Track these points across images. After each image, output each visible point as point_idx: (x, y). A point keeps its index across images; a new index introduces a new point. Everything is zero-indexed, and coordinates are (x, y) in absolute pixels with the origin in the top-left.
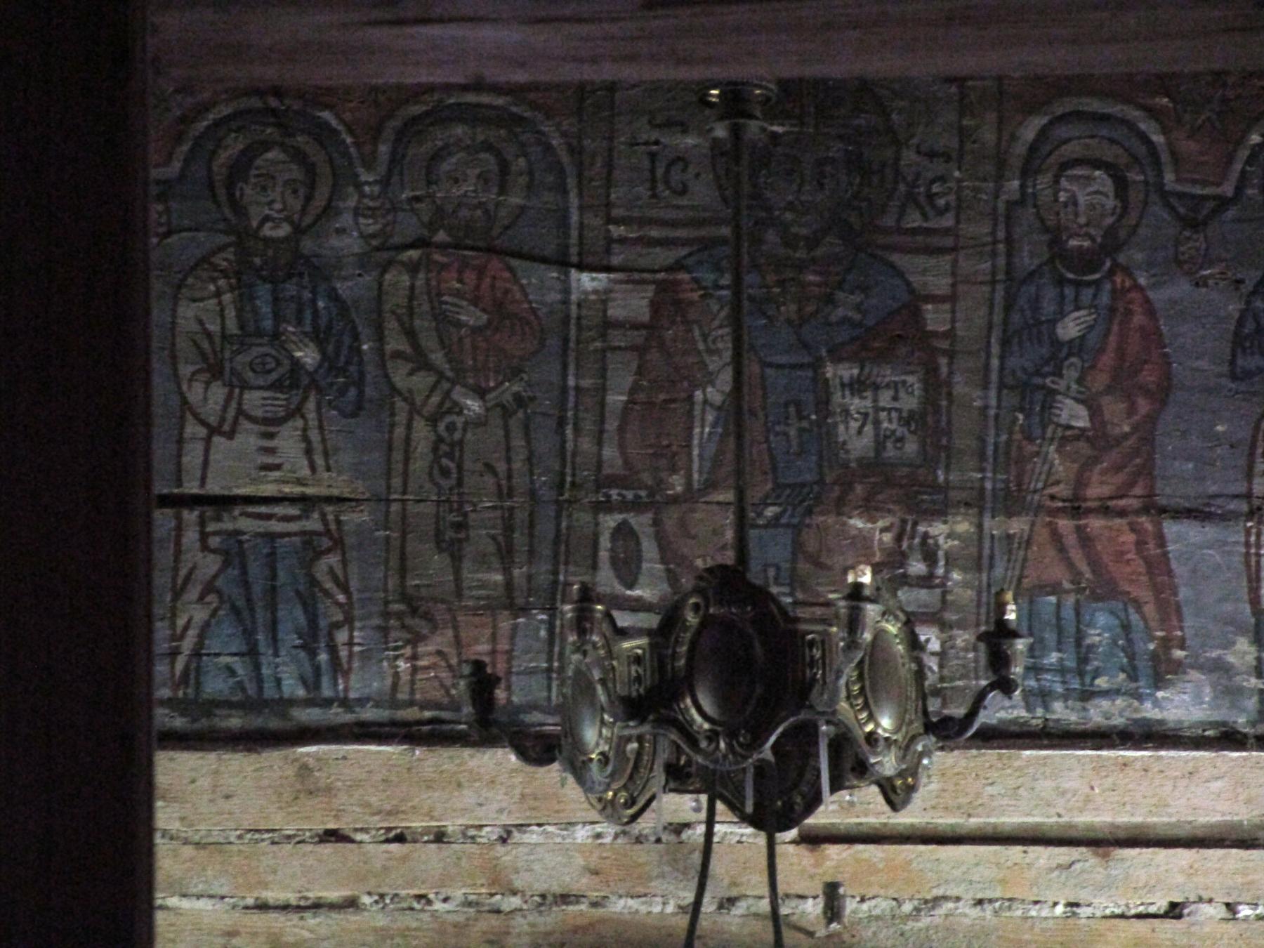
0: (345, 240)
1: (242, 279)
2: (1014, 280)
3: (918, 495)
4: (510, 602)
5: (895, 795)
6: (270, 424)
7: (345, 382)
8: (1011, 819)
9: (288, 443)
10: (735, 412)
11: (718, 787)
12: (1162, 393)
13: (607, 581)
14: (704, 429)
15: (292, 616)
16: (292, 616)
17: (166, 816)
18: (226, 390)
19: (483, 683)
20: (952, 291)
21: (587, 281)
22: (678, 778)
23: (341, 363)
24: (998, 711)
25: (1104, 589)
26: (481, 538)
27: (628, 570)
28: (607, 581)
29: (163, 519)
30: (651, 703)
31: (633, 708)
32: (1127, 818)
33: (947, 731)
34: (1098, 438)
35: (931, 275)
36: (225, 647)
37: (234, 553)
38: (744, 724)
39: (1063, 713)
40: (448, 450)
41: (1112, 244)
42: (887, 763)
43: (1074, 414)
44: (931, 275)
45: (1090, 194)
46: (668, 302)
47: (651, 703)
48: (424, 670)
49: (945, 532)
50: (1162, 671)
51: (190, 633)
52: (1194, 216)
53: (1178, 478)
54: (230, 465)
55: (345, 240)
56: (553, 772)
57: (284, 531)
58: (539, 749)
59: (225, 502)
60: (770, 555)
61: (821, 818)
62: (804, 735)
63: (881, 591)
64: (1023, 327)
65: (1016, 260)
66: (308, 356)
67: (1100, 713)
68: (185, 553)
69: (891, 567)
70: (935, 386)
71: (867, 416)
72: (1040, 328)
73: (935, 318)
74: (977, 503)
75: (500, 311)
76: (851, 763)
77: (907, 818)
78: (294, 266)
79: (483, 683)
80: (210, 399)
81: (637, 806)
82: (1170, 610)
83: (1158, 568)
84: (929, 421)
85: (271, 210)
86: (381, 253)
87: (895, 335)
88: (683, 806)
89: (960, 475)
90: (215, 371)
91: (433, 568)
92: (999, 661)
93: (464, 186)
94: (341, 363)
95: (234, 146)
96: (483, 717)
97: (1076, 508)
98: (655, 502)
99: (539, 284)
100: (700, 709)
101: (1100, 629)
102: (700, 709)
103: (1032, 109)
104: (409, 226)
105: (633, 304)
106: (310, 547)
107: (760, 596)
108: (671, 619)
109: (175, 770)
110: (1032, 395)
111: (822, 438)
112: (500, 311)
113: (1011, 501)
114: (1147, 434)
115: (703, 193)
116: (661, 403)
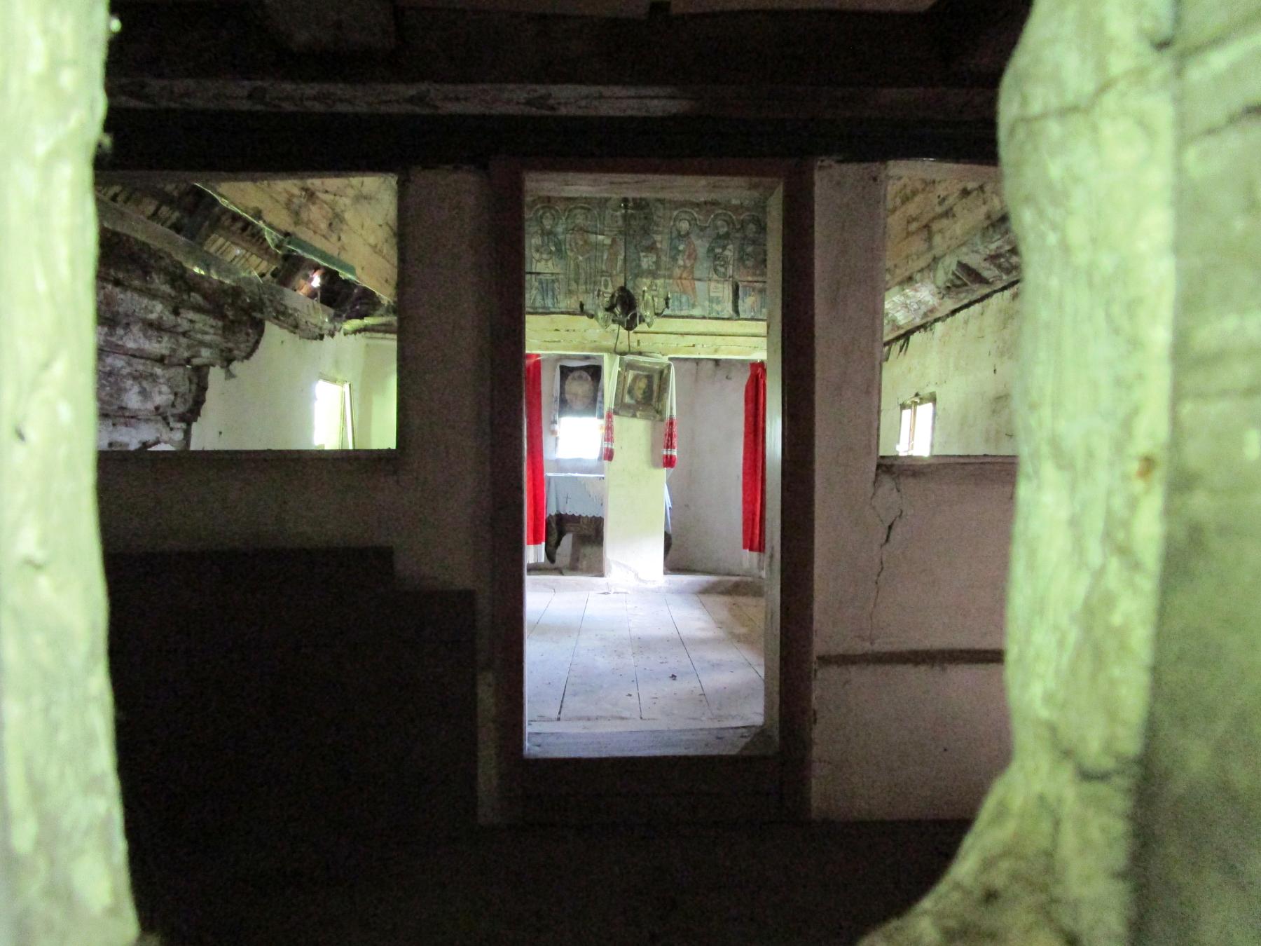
0: (560, 229)
1: (543, 234)
2: (672, 239)
3: (653, 274)
4: (587, 292)
5: (649, 325)
6: (547, 260)
7: (560, 252)
8: (669, 330)
9: (550, 263)
10: (625, 260)
11: (621, 323)
12: (695, 259)
13: (603, 288)
14: (620, 263)
15: (550, 293)
16: (550, 293)
17: (527, 326)
18: (603, 422)
19: (582, 305)
20: (661, 240)
21: (600, 237)
22: (614, 321)
23: (559, 250)
24: (667, 312)
25: (684, 292)
26: (582, 281)
27: (606, 286)
28: (603, 288)
29: (528, 277)
30: (610, 309)
31: (607, 310)
32: (686, 330)
33: (657, 314)
34: (685, 267)
35: (658, 238)
36: (539, 298)
37: (541, 282)
38: (625, 312)
39: (678, 313)
40: (577, 266)
41: (688, 234)
42: (648, 320)
43: (681, 262)
44: (658, 238)
45: (684, 226)
46: (614, 241)
47: (610, 309)
48: (573, 303)
49: (659, 282)
50: (694, 306)
51: (532, 296)
52: (702, 229)
53: (697, 274)
54: (539, 267)
55: (560, 229)
56: (593, 320)
57: (768, 496)
58: (591, 316)
59: (539, 274)
60: (629, 286)
61: (637, 329)
62: (635, 315)
63: (648, 292)
64: (674, 248)
65: (184, 388)
66: (553, 249)
67: (684, 313)
68: (531, 283)
69: (650, 287)
70: (659, 257)
71: (647, 262)
72: (676, 248)
73: (659, 245)
74: (664, 277)
75: (586, 242)
76: (642, 320)
77: (652, 329)
78: (550, 233)
79: (582, 305)
80: (537, 256)
81: (607, 326)
82: (695, 296)
83: (694, 289)
84: (657, 263)
85: (547, 224)
86: (566, 231)
87: (651, 248)
88: (615, 326)
89: (661, 272)
90: (537, 251)
91: (574, 286)
92: (667, 304)
93: (580, 220)
94: (559, 250)
95: (541, 212)
96: (582, 311)
97: (680, 278)
98: (611, 276)
99: (593, 238)
100: (618, 310)
101: (684, 299)
102: (618, 310)
103: (676, 208)
104: (571, 227)
105: (608, 241)
106: (553, 281)
107: (628, 292)
108: (613, 296)
109: (528, 318)
110: (674, 259)
111: (639, 266)
112: (586, 242)
113: (670, 277)
114: (692, 266)
115: (620, 223)
116: (612, 259)
